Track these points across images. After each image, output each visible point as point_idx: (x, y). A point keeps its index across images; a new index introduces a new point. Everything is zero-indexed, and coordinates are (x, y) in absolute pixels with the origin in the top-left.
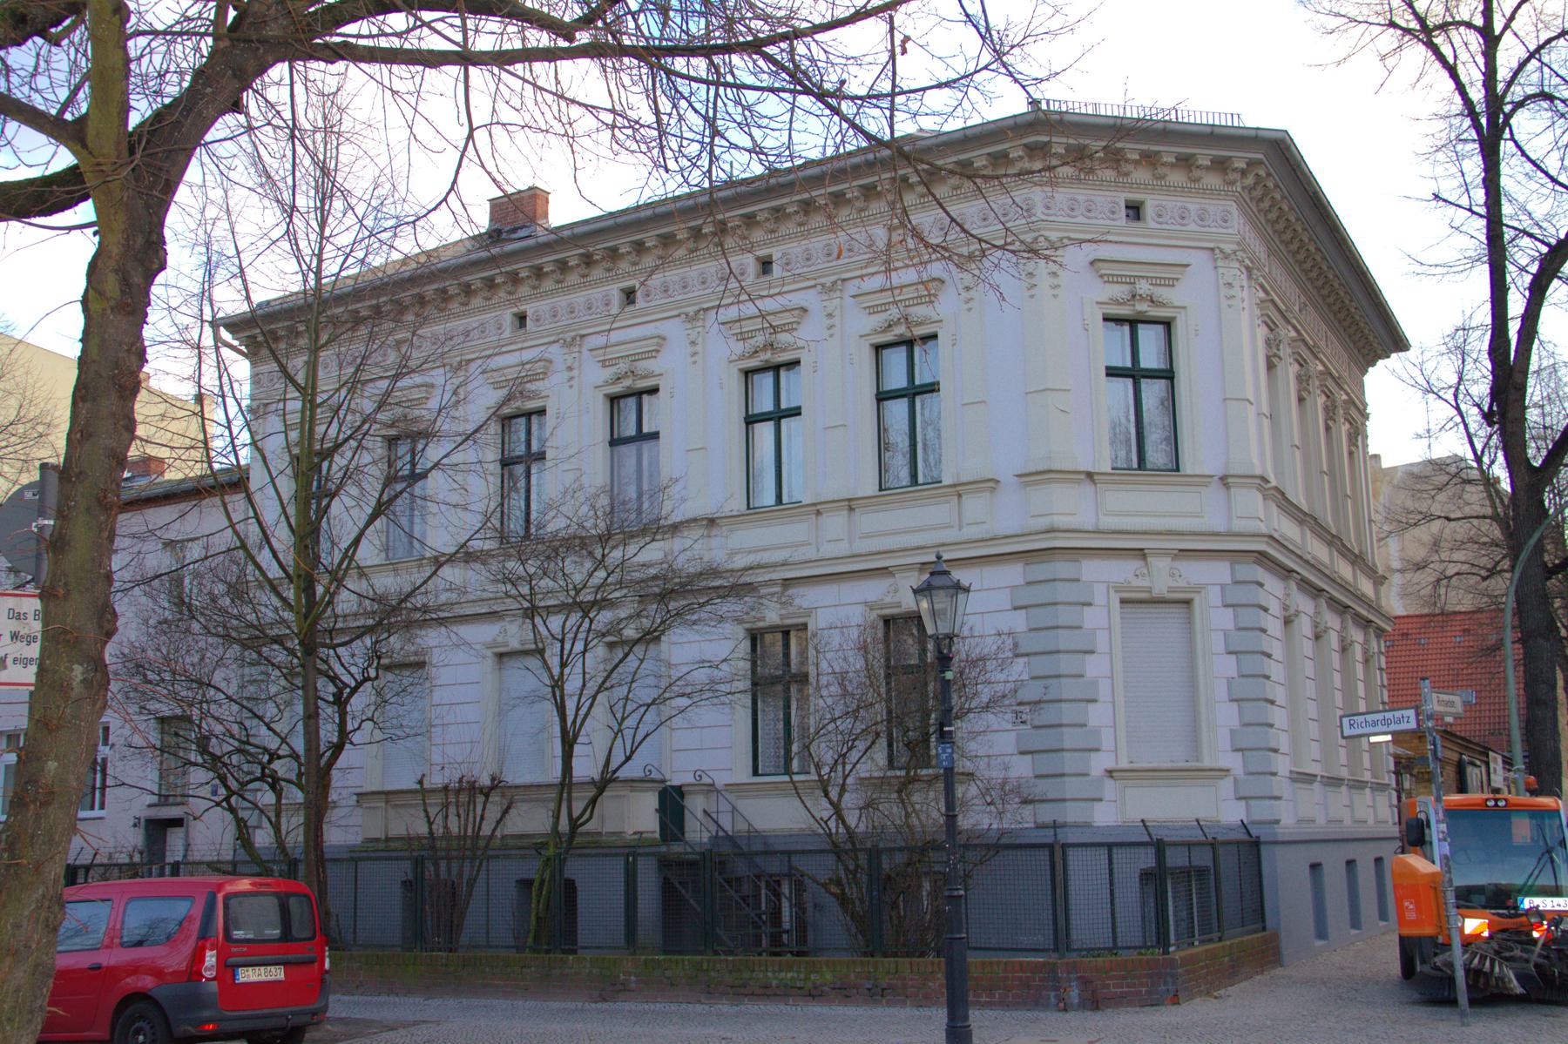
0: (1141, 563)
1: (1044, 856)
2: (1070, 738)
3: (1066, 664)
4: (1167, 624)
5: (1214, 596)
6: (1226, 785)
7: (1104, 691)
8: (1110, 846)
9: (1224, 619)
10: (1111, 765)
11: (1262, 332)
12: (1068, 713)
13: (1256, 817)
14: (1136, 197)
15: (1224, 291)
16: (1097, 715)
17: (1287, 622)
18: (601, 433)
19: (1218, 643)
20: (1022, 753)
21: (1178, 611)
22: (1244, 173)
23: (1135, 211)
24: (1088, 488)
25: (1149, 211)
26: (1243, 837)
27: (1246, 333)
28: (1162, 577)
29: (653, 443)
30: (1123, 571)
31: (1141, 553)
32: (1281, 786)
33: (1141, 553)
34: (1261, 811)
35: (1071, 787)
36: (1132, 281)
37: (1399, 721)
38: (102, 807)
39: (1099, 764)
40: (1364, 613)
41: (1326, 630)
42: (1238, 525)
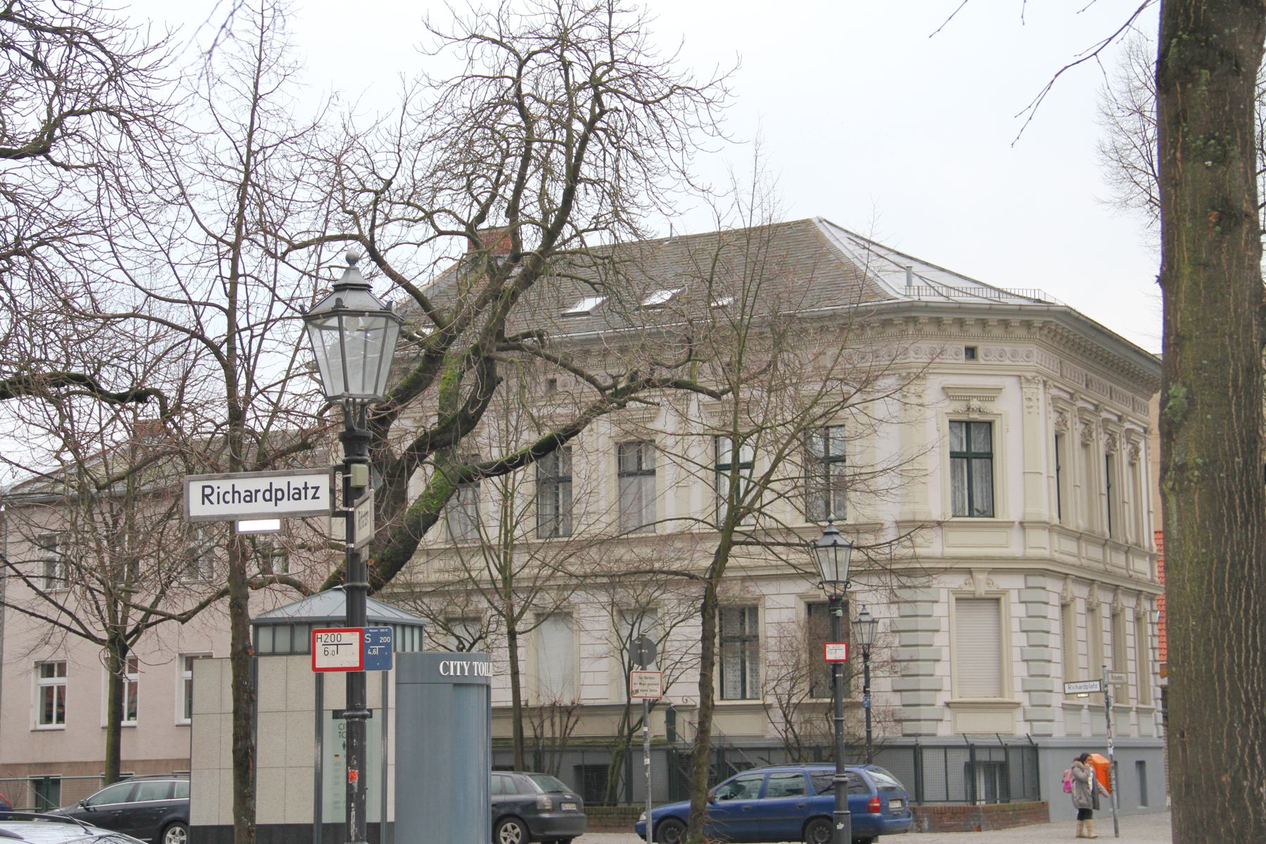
0: (968, 576)
1: (910, 754)
2: (924, 683)
3: (922, 638)
4: (982, 619)
5: (1014, 596)
6: (1018, 714)
7: (945, 655)
8: (946, 748)
9: (1018, 610)
10: (949, 699)
11: (1054, 416)
12: (923, 668)
13: (1036, 732)
14: (971, 344)
15: (1026, 403)
16: (941, 669)
17: (1064, 606)
18: (613, 468)
19: (1015, 626)
20: (895, 691)
21: (991, 607)
22: (1041, 329)
23: (971, 353)
24: (938, 531)
25: (980, 353)
26: (1026, 743)
27: (1043, 424)
28: (982, 585)
29: (650, 479)
30: (958, 582)
31: (969, 571)
32: (1058, 714)
33: (969, 571)
34: (1039, 728)
35: (925, 712)
36: (968, 398)
37: (298, 495)
38: (61, 718)
39: (944, 697)
40: (1133, 587)
41: (1098, 605)
42: (1031, 553)
